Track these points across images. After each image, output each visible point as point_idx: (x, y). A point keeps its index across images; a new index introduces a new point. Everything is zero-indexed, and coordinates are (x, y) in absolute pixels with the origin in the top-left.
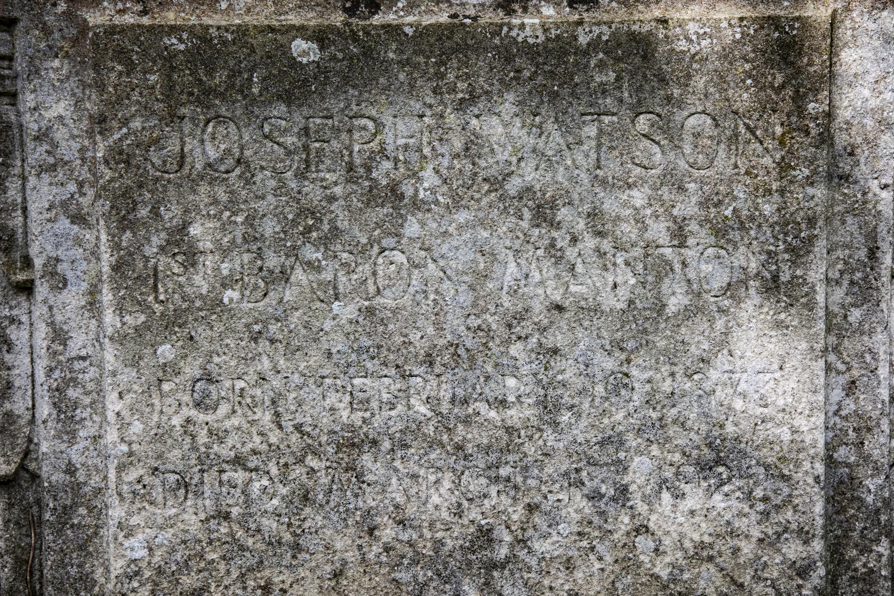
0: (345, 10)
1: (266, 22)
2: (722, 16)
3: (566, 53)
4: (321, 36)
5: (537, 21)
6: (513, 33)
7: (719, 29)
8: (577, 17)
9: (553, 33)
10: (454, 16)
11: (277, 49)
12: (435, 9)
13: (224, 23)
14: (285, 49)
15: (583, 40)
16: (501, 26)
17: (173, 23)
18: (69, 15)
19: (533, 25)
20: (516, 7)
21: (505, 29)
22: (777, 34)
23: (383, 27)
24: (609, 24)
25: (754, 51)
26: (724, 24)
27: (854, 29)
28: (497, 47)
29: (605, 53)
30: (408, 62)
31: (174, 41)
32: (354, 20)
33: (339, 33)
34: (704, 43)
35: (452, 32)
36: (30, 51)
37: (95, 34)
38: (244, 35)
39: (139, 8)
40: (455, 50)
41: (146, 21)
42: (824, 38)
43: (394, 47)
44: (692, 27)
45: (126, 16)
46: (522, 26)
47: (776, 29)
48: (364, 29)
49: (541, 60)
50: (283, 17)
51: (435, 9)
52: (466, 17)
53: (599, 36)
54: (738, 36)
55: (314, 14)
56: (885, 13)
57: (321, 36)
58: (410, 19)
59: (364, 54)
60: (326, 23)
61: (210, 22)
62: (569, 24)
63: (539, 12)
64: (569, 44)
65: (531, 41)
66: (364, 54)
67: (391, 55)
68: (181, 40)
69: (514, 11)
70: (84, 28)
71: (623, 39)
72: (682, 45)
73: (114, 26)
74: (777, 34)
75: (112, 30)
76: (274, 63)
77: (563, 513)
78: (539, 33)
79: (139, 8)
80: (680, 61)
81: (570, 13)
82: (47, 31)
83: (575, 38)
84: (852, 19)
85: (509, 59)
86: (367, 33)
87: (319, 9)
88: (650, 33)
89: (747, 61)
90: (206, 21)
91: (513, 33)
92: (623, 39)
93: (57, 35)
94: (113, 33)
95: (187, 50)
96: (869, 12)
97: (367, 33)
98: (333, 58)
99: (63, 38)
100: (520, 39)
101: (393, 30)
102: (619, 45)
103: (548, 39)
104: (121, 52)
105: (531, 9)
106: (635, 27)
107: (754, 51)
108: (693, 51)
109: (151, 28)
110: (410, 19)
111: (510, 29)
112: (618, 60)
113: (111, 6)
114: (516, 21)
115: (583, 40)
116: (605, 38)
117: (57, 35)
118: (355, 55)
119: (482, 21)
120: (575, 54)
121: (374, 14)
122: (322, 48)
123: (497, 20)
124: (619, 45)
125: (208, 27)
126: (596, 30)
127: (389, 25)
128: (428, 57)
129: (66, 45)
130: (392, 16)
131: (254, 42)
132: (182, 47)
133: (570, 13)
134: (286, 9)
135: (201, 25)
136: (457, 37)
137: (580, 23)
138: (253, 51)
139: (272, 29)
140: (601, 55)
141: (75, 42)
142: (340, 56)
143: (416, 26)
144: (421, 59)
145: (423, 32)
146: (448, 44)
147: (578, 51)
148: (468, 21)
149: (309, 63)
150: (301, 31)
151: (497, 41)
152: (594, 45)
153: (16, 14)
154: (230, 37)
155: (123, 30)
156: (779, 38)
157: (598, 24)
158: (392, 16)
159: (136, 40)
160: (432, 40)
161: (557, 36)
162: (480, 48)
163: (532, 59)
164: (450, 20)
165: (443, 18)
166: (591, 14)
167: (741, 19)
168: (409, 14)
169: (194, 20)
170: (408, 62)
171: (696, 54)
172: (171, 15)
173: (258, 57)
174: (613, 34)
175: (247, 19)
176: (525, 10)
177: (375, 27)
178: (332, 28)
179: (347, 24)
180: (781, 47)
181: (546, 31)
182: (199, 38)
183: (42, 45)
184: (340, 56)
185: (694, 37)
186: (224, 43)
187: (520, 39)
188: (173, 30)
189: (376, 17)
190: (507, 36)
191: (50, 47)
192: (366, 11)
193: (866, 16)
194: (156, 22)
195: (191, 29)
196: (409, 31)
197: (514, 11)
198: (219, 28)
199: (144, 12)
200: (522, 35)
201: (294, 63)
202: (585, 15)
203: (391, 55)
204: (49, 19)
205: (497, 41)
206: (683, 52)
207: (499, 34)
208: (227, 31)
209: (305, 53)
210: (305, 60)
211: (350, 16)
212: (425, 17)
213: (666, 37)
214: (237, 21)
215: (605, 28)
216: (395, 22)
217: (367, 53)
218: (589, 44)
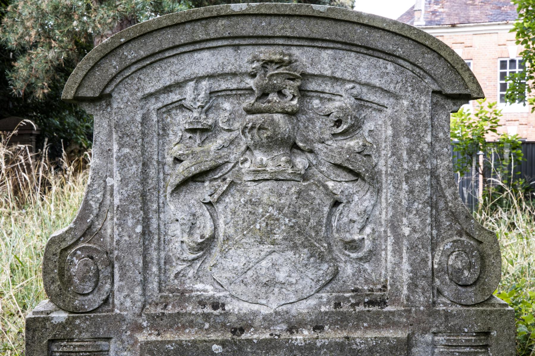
0: (232, 332)
1: (203, 339)
2: (369, 336)
3: (312, 349)
4: (223, 343)
5: (301, 337)
6: (293, 342)
7: (367, 341)
8: (316, 335)
9: (308, 342)
10: (271, 335)
11: (207, 348)
12: (265, 331)
13: (188, 339)
14: (210, 348)
15: (319, 344)
16: (289, 339)
17: (169, 339)
18: (131, 336)
19: (300, 339)
20: (294, 331)
21: (290, 340)
22: (388, 343)
23: (246, 340)
24: (328, 339)
25: (380, 349)
26: (369, 339)
27: (416, 340)
28: (287, 347)
29: (327, 349)
30: (255, 352)
31: (170, 346)
32: (235, 337)
33: (230, 342)
34: (362, 346)
35: (271, 342)
36: (116, 349)
37: (141, 344)
38: (195, 343)
39: (157, 333)
40: (272, 348)
41: (159, 338)
42: (405, 345)
43: (250, 347)
44: (358, 340)
45: (152, 336)
46: (296, 339)
47: (388, 341)
48: (239, 340)
49: (303, 351)
50: (209, 336)
51: (265, 331)
52: (276, 335)
53: (324, 343)
54: (374, 344)
55: (219, 334)
56: (427, 335)
57: (223, 343)
58: (255, 336)
59: (239, 350)
60: (225, 338)
61: (183, 339)
62: (313, 339)
63: (302, 333)
64: (314, 346)
65: (300, 345)
66: (239, 350)
67: (249, 350)
68: (172, 346)
69: (293, 333)
70: (136, 342)
71: (333, 344)
72: (354, 346)
73: (148, 342)
74: (388, 343)
75: (147, 343)
76: (206, 353)
77: (449, 311)
78: (303, 342)
79: (157, 333)
80: (354, 352)
81: (314, 333)
82: (123, 342)
83: (316, 344)
84: (415, 337)
85: (292, 351)
86: (240, 342)
87: (222, 332)
88: (343, 342)
89: (378, 353)
90: (182, 338)
91: (293, 342)
92: (333, 344)
93: (126, 343)
94: (148, 344)
95: (174, 349)
96: (421, 335)
97: (240, 342)
98: (227, 351)
99: (129, 344)
100: (296, 344)
101: (249, 341)
102: (332, 346)
103: (306, 344)
104: (150, 351)
105: (299, 332)
106: (337, 340)
107: (380, 349)
108: (358, 349)
109: (161, 342)
110: (255, 336)
111: (292, 340)
112: (331, 352)
113: (146, 332)
114: (294, 337)
115: (319, 344)
116: (326, 344)
117: (126, 343)
118: (235, 350)
119: (282, 337)
120: (316, 349)
121: (242, 333)
122: (223, 348)
123: (287, 337)
124: (332, 346)
125: (182, 341)
126: (323, 341)
127: (248, 339)
128: (262, 351)
129: (129, 347)
130: (249, 335)
131: (199, 346)
132: (172, 348)
133: (314, 333)
134: (210, 332)
135: (179, 340)
136: (273, 343)
137: (317, 338)
138: (198, 349)
139: (205, 341)
140: (325, 350)
141: (133, 345)
142: (230, 350)
143: (258, 339)
144: (260, 351)
145: (260, 342)
146: (269, 346)
147: (317, 348)
148: (277, 337)
149: (218, 353)
150: (216, 342)
151: (287, 345)
152: (323, 346)
153: (112, 336)
154: (190, 344)
155: (151, 343)
156: (389, 345)
157: (324, 339)
158: (249, 335)
159: (156, 346)
160: (264, 344)
161: (309, 343)
162: (281, 347)
163: (300, 351)
164: (270, 337)
165: (267, 336)
166: (321, 334)
167: (375, 338)
168: (255, 333)
169: (177, 338)
170: (255, 352)
171: (360, 350)
172: (168, 335)
173: (200, 351)
174: (329, 342)
175: (196, 336)
176: (297, 332)
177: (243, 340)
178: (227, 341)
179: (233, 339)
180: (390, 348)
181: (305, 341)
182: (179, 345)
183: (121, 347)
184: (230, 350)
185: (359, 344)
186: (188, 346)
187: (296, 344)
188: (169, 342)
189: (243, 335)
190: (291, 343)
191: (124, 348)
192: (239, 332)
193: (420, 336)
194: (163, 339)
195: (176, 342)
196: (255, 341)
197: (293, 333)
198: (186, 341)
199: (158, 335)
200: (296, 343)
201: (213, 353)
202: (319, 334)
203: (249, 350)
204: (124, 337)
205: (287, 345)
206: (355, 349)
207: (288, 342)
208: (189, 342)
209: (217, 350)
210: (217, 352)
211: (234, 335)
212: (261, 335)
213: (349, 343)
214: (193, 338)
215: (326, 340)
216: (250, 338)
217: (240, 349)
218: (321, 346)
